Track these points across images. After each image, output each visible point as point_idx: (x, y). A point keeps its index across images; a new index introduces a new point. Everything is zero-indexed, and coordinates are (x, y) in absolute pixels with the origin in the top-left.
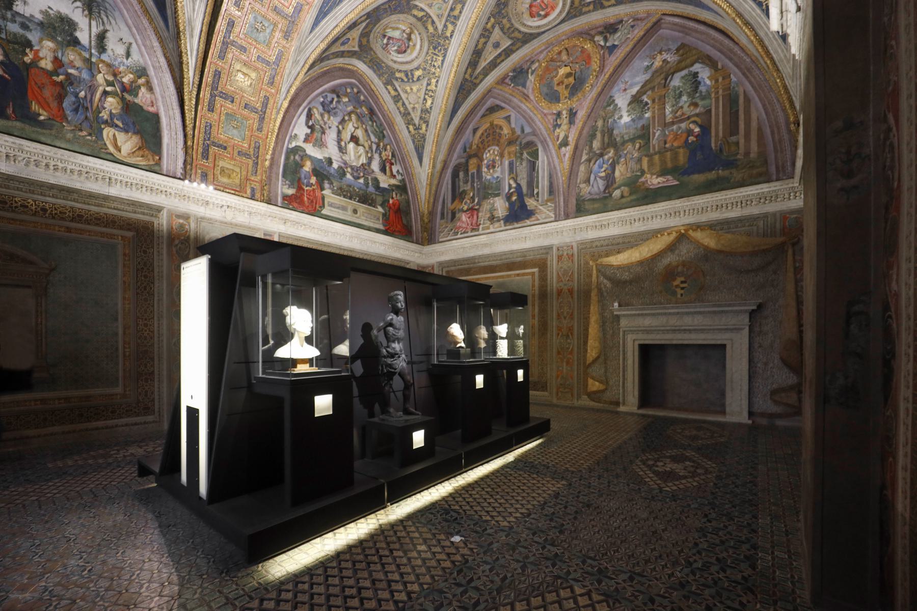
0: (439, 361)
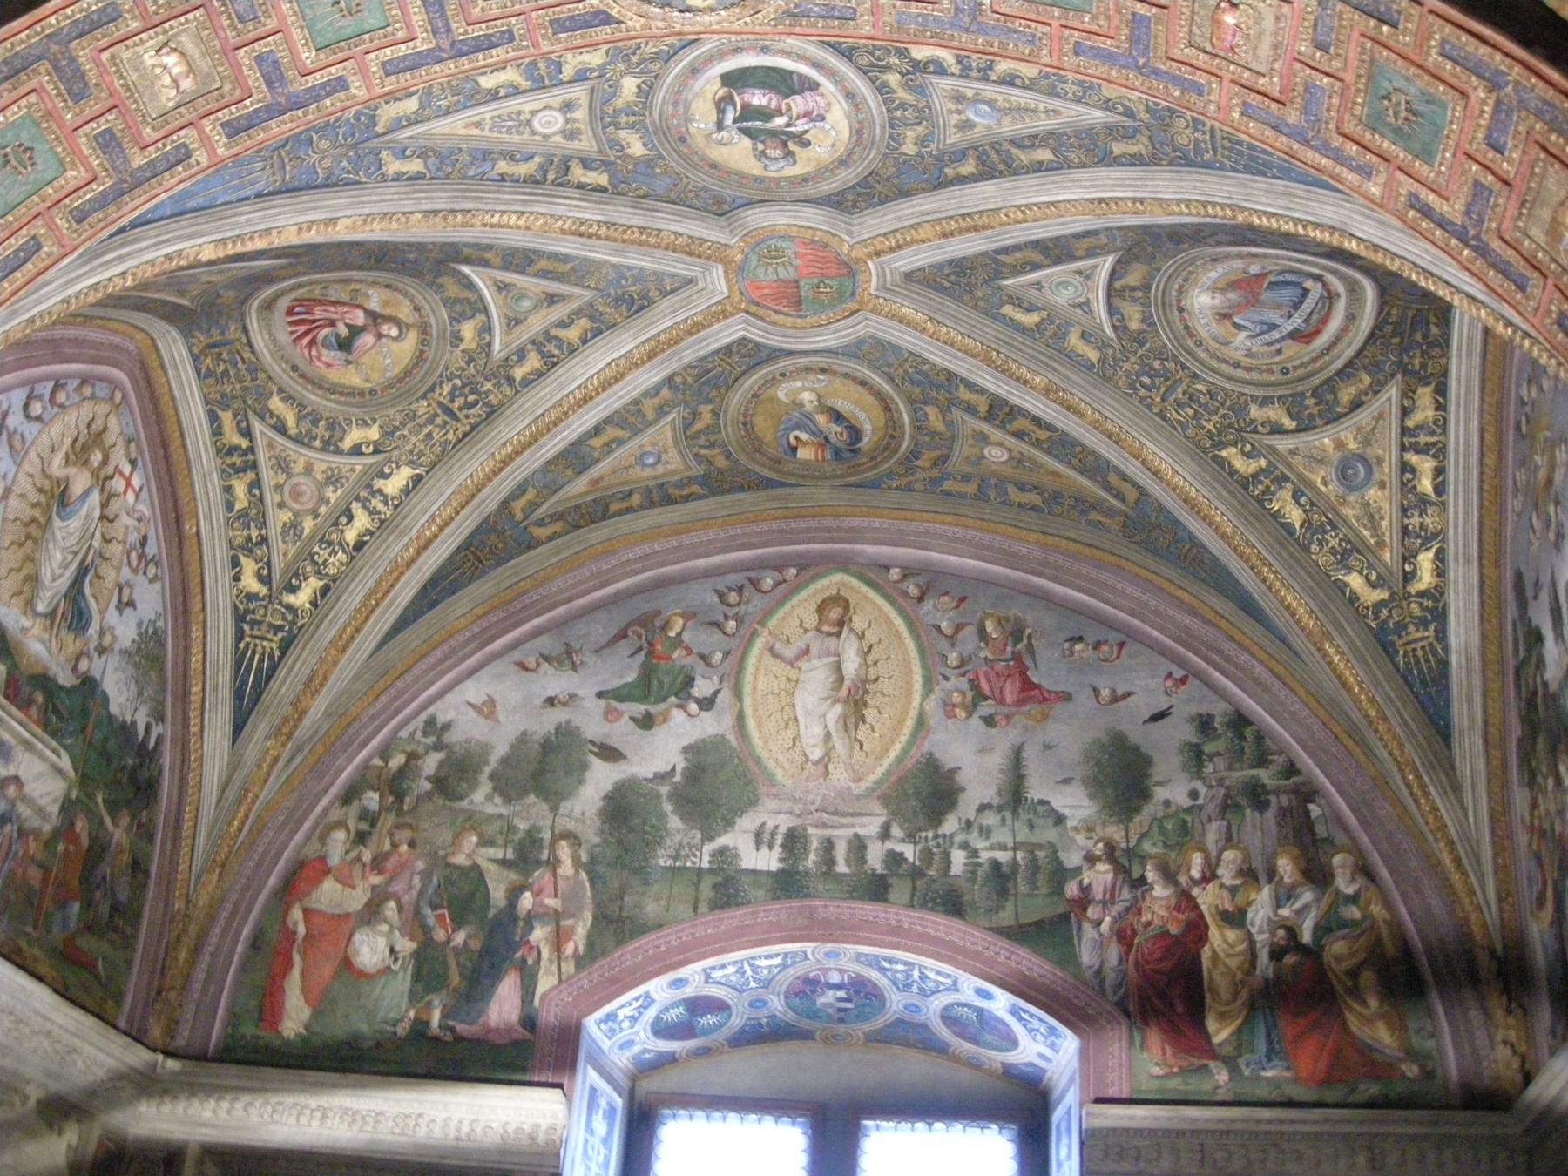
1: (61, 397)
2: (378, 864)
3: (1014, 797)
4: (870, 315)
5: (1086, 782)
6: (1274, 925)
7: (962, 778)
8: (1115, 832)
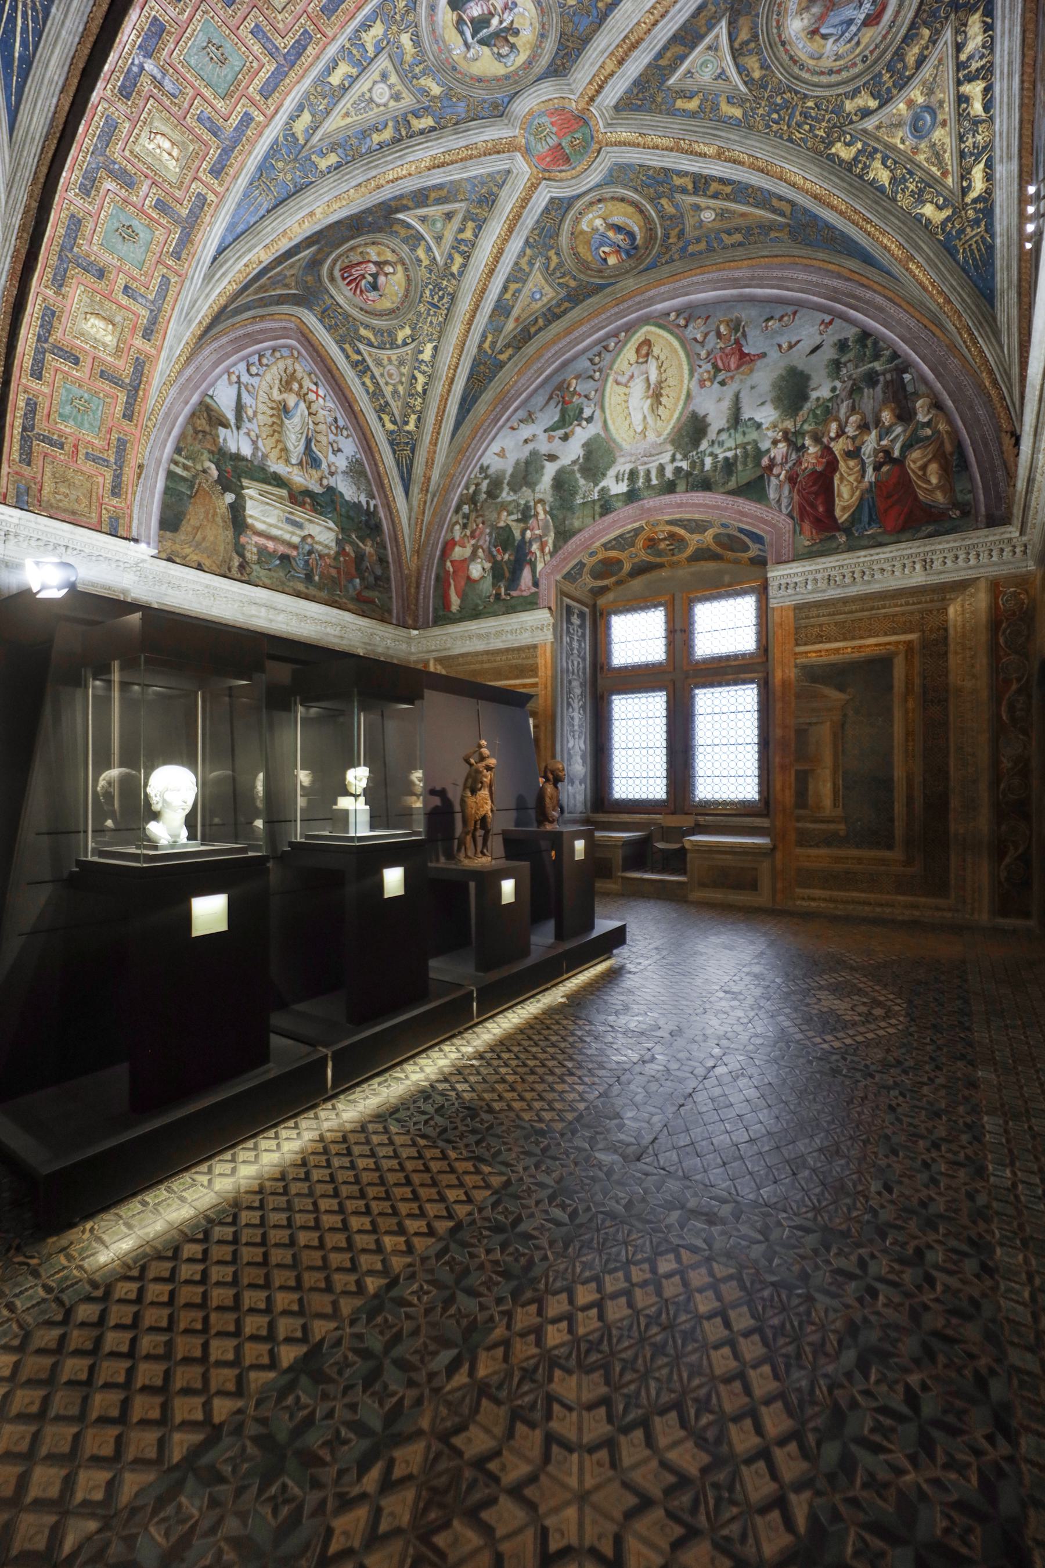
0: (308, 837)
1: (265, 361)
2: (473, 536)
3: (736, 420)
4: (609, 149)
5: (772, 401)
6: (876, 452)
7: (709, 419)
8: (789, 424)
